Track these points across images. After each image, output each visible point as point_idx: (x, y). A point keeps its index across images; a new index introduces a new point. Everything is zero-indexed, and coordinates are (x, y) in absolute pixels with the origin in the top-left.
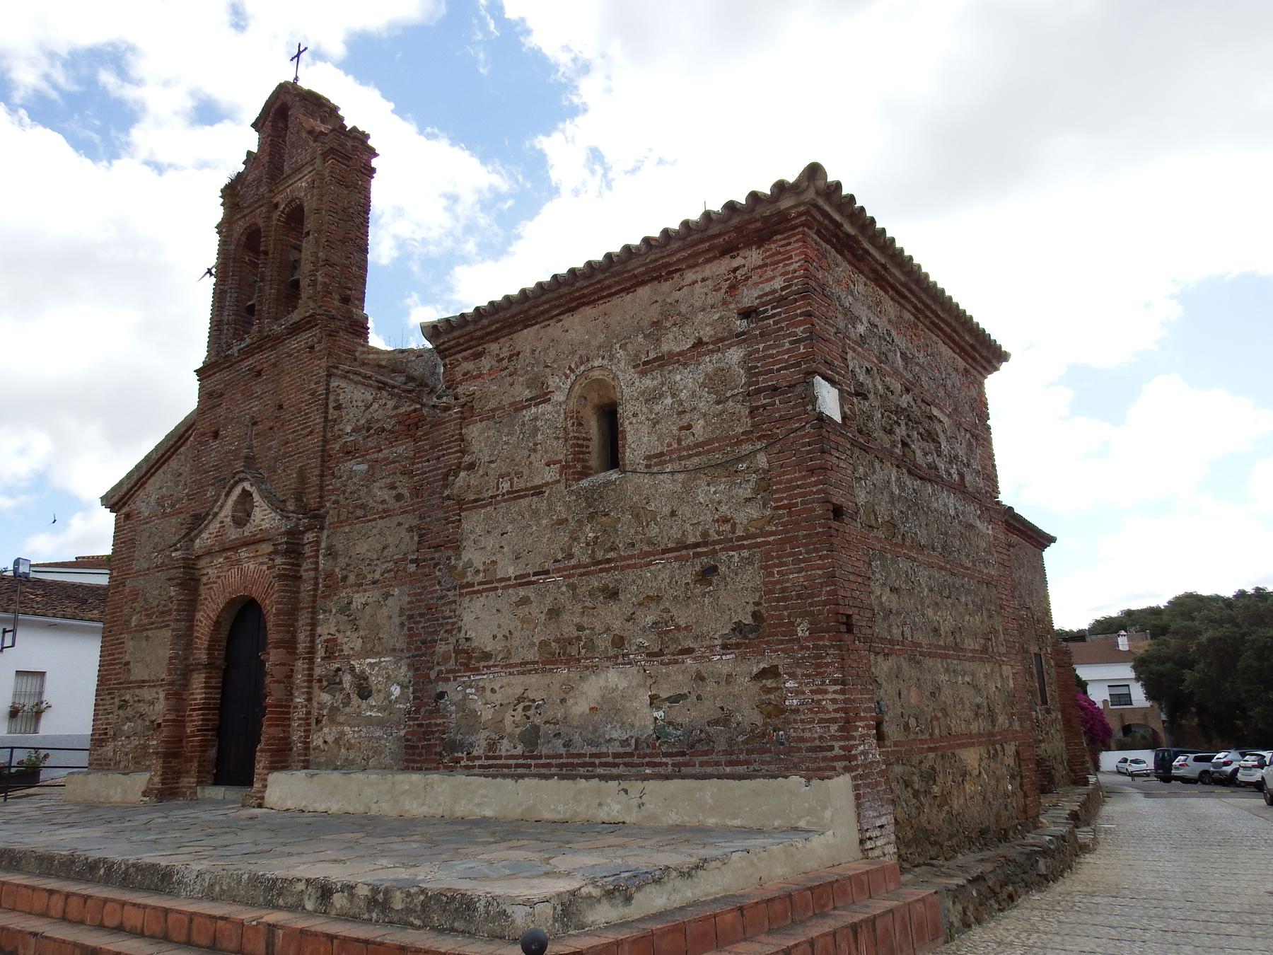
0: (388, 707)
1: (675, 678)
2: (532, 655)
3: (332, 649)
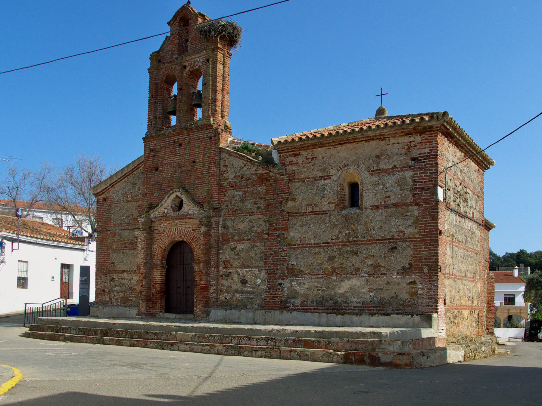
0: (257, 286)
1: (381, 281)
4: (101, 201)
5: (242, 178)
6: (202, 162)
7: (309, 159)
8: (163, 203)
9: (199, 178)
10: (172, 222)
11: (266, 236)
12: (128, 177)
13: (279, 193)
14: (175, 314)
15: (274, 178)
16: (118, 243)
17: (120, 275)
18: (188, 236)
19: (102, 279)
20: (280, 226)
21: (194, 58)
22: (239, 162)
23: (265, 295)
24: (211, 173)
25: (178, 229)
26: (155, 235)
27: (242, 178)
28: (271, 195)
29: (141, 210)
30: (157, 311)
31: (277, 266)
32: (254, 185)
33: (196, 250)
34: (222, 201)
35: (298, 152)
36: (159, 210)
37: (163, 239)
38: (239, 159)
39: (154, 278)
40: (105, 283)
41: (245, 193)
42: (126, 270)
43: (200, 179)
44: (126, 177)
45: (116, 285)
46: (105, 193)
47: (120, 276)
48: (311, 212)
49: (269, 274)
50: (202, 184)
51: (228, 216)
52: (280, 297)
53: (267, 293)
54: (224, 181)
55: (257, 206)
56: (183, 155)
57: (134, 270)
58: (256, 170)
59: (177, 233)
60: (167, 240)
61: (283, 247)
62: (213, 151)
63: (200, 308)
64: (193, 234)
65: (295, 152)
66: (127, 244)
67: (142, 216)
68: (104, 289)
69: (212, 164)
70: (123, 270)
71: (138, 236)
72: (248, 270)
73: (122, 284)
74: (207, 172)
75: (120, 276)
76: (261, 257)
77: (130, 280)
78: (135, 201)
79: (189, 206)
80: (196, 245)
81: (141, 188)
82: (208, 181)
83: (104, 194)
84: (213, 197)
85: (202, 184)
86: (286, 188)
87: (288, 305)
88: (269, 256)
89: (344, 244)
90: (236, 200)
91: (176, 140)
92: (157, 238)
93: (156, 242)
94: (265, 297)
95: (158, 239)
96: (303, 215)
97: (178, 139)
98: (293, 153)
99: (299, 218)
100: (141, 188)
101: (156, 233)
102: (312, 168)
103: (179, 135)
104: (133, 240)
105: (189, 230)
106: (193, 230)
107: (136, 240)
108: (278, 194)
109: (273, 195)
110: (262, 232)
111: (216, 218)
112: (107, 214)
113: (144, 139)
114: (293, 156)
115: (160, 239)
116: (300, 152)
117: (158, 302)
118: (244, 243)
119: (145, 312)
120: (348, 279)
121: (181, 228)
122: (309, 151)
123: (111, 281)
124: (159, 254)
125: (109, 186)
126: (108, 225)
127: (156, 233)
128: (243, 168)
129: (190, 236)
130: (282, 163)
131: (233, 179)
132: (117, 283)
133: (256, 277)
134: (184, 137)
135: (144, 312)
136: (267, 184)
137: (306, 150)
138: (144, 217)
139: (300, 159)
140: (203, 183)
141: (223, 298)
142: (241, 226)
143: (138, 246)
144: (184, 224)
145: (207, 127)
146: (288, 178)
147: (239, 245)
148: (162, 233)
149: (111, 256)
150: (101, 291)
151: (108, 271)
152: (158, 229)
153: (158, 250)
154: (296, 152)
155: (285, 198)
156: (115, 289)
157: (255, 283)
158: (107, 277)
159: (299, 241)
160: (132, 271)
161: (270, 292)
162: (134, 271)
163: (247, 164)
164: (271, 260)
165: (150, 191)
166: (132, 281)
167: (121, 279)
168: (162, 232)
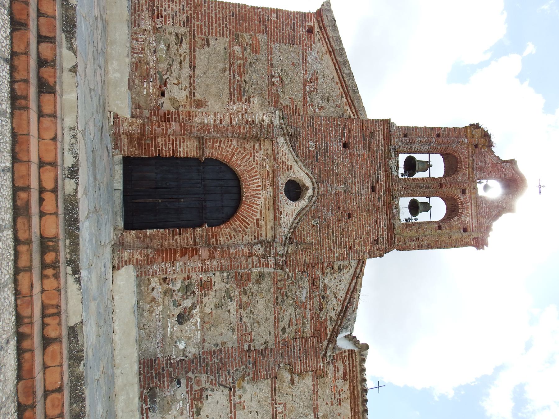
4: (308, 22)
5: (323, 297)
6: (348, 230)
7: (340, 394)
8: (300, 163)
9: (328, 228)
10: (270, 180)
11: (246, 348)
12: (339, 85)
13: (302, 358)
14: (121, 188)
15: (320, 347)
16: (240, 59)
17: (187, 59)
18: (248, 212)
19: (180, 12)
20: (259, 368)
21: (471, 207)
22: (343, 290)
23: (161, 359)
24: (334, 248)
25: (259, 190)
26: (251, 144)
27: (323, 297)
28: (300, 347)
29: (290, 110)
30: (126, 148)
31: (204, 373)
32: (313, 318)
33: (228, 230)
34: (295, 269)
35: (348, 377)
36: (290, 155)
37: (245, 160)
38: (346, 290)
39: (183, 142)
40: (173, 19)
41: (304, 305)
42: (196, 75)
43: (327, 228)
44: (340, 81)
46: (320, 33)
47: (185, 57)
48: (276, 411)
49: (193, 361)
50: (320, 233)
51: (274, 281)
52: (160, 385)
53: (164, 362)
54: (321, 269)
55: (287, 326)
56: (360, 195)
58: (331, 318)
59: (254, 190)
60: (244, 168)
61: (231, 378)
62: (361, 248)
63: (135, 256)
64: (252, 222)
65: (348, 374)
66: (238, 78)
67: (282, 121)
68: (162, 17)
69: (344, 248)
70: (196, 67)
71: (251, 102)
72: (198, 324)
73: (171, 63)
74: (335, 240)
75: (185, 57)
76: (217, 345)
77: (179, 83)
78: (304, 99)
79: (292, 213)
80: (235, 230)
81: (323, 113)
82: (323, 242)
83: (319, 30)
84: (302, 254)
85: (320, 233)
86: (306, 367)
87: (149, 400)
88: (219, 357)
90: (296, 292)
91: (381, 181)
92: (246, 146)
93: (241, 145)
94: (159, 360)
95: (244, 151)
96: (272, 400)
97: (381, 184)
98: (348, 371)
99: (270, 395)
100: (323, 113)
101: (254, 146)
102: (329, 403)
103: (386, 187)
104: (244, 91)
105: (257, 212)
106: (257, 220)
107: (244, 99)
108: (300, 357)
109: (300, 350)
110: (252, 340)
111: (273, 264)
112: (289, 35)
113: (389, 120)
114: (344, 371)
115: (246, 155)
116: (348, 381)
117: (142, 149)
118: (237, 312)
119: (121, 132)
121: (260, 198)
122: (348, 392)
123: (177, 35)
124: (221, 153)
125: (330, 45)
126: (271, 35)
127: (254, 146)
128: (336, 297)
129: (249, 216)
130: (337, 356)
131: (322, 283)
132: (173, 50)
134: (383, 195)
135: (121, 128)
136: (313, 339)
137: (350, 390)
138: (281, 124)
139: (340, 383)
140: (321, 235)
141: (153, 285)
142: (261, 305)
143: (234, 103)
144: (267, 204)
145: (391, 237)
146: (319, 369)
147: (235, 304)
148: (254, 158)
149: (220, 39)
150: (158, 10)
151: (194, 30)
152: (261, 150)
153: (228, 149)
154: (348, 376)
155: (295, 370)
156: (162, 46)
157: (179, 340)
158: (184, 26)
159: (239, 400)
160: (194, 89)
161: (167, 367)
162: (194, 93)
163: (339, 303)
164: (213, 362)
165: (316, 133)
166: (176, 88)
167: (181, 62)
168: (256, 158)
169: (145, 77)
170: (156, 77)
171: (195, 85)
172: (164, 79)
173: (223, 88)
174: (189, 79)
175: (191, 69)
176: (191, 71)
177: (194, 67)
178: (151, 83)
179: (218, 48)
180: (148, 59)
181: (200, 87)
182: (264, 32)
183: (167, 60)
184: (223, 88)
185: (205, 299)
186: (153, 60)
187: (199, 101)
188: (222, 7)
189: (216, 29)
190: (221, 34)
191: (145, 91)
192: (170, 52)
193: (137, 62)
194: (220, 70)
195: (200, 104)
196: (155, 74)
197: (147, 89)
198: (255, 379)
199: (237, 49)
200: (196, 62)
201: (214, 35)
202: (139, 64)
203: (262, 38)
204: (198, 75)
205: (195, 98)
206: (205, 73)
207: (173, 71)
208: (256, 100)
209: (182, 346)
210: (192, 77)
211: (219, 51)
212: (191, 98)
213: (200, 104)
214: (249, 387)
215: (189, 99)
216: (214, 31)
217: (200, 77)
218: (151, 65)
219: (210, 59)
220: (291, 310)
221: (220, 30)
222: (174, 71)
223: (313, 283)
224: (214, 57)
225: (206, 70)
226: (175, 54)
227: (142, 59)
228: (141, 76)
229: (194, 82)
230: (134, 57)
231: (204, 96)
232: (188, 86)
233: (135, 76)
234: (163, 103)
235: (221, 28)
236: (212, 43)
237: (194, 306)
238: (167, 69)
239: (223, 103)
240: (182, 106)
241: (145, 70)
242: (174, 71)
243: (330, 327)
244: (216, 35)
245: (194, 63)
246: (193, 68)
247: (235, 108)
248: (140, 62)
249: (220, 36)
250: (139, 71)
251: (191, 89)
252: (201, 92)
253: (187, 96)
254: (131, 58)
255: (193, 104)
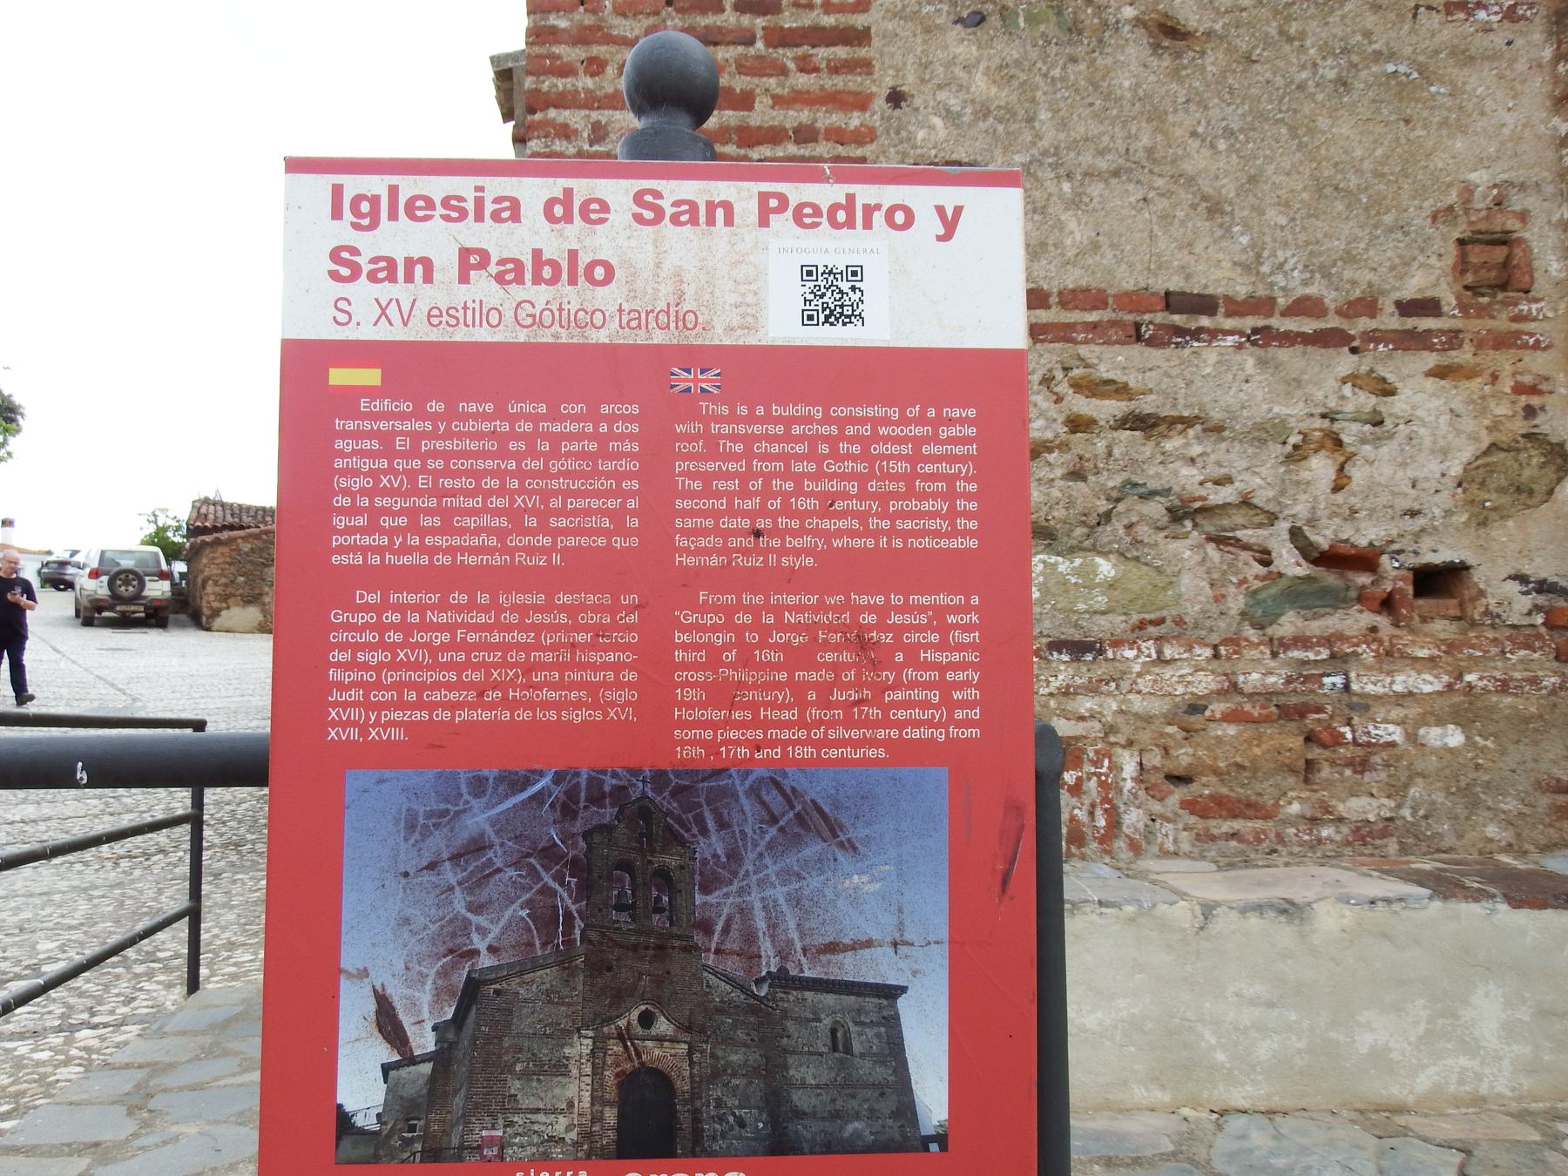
0: (757, 1130)
1: (877, 1125)
2: (826, 1115)
3: (719, 1103)
17: (1113, 361)
42: (1241, 290)
45: (517, 1134)
57: (1414, 285)
70: (1175, 284)
89: (842, 1087)
120: (852, 1122)
133: (757, 1120)
139: (791, 998)
142: (734, 1058)
156: (517, 1140)
160: (1368, 305)
162: (1408, 308)
167: (1142, 423)
169: (546, 1156)
170: (1302, 641)
171: (1331, 298)
172: (1303, 570)
173: (1326, 51)
174: (1283, 354)
175: (1196, 334)
176: (1214, 334)
177: (1172, 301)
178: (1367, 684)
179: (980, 84)
180: (1157, 707)
181: (1349, 258)
182: (500, 1039)
183: (1137, 542)
184: (1326, 51)
185: (729, 1105)
186: (1161, 661)
187: (1462, 266)
188: (582, 37)
189: (799, 98)
190: (841, 52)
191: (1433, 735)
192: (1059, 513)
193: (1190, 805)
194: (1175, 74)
195: (570, 1104)
196: (1278, 647)
197: (1422, 721)
198: (786, 1067)
199: (518, 1067)
200: (1128, 280)
201: (855, 120)
202: (1205, 787)
203: (507, 1042)
204: (1246, 268)
205: (1449, 300)
206: (1215, 208)
207: (1226, 494)
208: (567, 1051)
209: (761, 1125)
210: (546, 1112)
211: (1002, 74)
212: (1453, 339)
213: (570, 1104)
214: (792, 1072)
215: (1463, 355)
216: (827, 119)
217: (1257, 249)
218: (1205, 683)
219: (1087, 159)
220: (739, 1032)
221: (806, 66)
222: (1225, 480)
223: (719, 1011)
224: (1063, 125)
225: (1186, 197)
226: (1077, 475)
227: (1155, 759)
228: (1310, 765)
229: (1306, 306)
230: (1149, 834)
231: (1420, 220)
232: (1345, 363)
233: (1314, 821)
234: (1521, 578)
235: (787, 56)
236: (513, 1091)
237: (734, 1114)
238: (1219, 540)
239: (1464, 57)
240: (1530, 412)
241: (1248, 731)
242: (1225, 480)
243: (752, 1001)
244: (861, 102)
245: (1135, 300)
246: (537, 1111)
247: (575, 1072)
248: (1179, 779)
249: (865, 66)
250: (1264, 789)
251: (1374, 337)
252: (1388, 251)
253: (1440, 373)
254: (1165, 854)
255: (1502, 323)
